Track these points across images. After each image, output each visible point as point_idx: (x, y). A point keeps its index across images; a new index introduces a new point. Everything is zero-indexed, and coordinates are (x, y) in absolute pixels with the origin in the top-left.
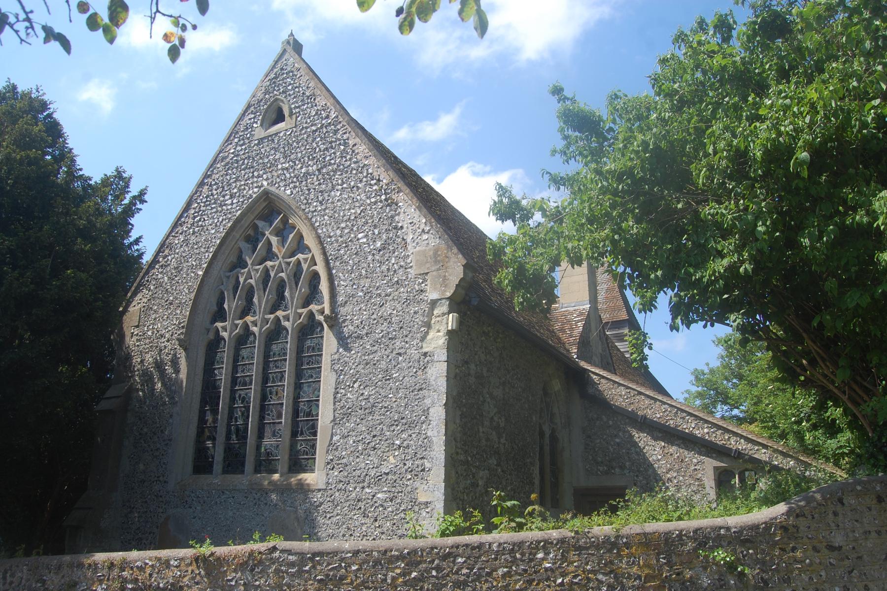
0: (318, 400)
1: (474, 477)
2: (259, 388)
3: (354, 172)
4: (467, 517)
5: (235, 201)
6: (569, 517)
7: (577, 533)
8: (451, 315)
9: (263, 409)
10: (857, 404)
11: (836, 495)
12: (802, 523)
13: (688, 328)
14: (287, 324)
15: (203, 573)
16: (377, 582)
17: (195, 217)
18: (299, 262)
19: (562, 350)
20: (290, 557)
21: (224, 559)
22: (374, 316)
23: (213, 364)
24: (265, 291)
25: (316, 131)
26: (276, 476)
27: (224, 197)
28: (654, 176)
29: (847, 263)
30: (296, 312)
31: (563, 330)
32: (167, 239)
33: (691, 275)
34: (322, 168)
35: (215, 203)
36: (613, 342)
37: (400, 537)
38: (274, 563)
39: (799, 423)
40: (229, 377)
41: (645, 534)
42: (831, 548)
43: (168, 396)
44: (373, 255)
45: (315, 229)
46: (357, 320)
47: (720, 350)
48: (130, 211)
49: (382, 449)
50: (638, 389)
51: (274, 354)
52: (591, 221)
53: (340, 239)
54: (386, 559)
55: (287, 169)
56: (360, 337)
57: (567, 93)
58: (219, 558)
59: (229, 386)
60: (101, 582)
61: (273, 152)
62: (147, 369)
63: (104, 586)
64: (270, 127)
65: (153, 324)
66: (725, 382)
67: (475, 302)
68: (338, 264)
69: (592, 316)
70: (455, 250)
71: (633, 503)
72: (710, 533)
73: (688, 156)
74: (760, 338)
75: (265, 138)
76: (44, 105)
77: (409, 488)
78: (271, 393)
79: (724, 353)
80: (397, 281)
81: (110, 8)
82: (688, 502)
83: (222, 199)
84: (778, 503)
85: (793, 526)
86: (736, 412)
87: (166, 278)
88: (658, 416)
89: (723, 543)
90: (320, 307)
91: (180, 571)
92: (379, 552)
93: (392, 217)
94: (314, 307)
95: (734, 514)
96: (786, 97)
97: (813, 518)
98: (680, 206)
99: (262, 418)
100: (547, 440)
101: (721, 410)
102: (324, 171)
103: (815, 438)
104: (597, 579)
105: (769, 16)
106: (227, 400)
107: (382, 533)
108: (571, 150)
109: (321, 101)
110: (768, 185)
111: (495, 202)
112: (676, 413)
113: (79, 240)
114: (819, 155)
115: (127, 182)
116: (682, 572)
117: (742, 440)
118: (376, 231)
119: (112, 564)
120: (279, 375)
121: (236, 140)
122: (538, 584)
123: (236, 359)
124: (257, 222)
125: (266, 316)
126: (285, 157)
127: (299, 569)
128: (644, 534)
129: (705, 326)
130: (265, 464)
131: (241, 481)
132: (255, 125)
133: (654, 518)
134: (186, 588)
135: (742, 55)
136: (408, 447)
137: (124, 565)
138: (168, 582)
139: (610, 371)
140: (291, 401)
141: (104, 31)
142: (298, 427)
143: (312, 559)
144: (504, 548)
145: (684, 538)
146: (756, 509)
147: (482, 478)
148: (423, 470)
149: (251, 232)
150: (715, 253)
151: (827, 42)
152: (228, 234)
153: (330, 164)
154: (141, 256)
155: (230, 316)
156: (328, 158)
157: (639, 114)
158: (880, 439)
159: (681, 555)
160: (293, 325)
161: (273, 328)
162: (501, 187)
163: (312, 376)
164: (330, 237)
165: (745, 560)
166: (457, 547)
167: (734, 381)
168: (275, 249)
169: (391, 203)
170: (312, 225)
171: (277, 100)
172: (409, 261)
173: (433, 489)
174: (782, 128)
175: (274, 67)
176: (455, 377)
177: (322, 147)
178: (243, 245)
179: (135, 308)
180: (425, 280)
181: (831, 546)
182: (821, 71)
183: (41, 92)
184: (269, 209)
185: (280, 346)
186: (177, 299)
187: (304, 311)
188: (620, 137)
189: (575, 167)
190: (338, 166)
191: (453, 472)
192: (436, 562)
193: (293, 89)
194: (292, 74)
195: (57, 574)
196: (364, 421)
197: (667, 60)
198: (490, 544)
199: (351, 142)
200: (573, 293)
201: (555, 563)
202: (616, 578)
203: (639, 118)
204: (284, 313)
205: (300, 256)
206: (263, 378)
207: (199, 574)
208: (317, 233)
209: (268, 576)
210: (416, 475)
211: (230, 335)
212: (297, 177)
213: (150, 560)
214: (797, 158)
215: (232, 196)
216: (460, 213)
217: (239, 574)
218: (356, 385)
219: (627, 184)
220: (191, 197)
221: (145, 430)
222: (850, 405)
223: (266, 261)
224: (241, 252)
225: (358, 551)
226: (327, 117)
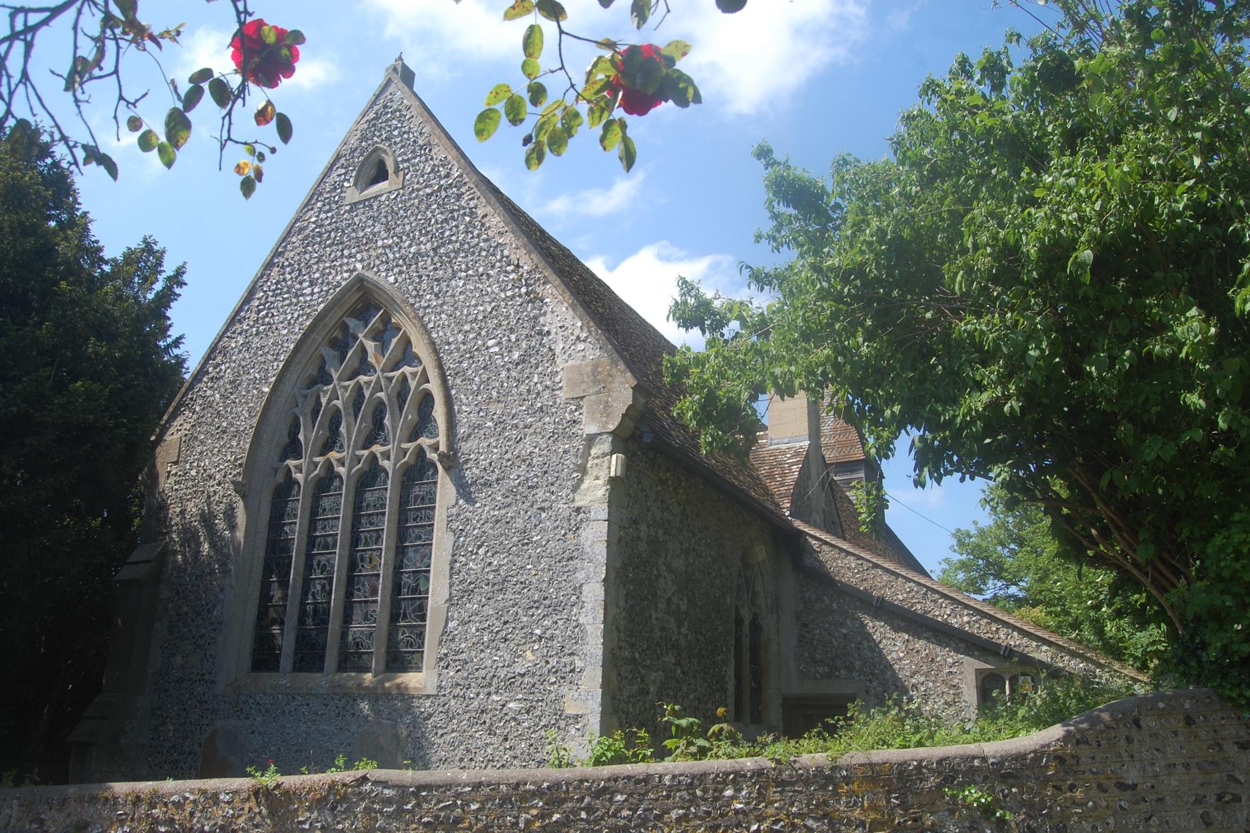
0: (428, 571)
1: (643, 680)
2: (346, 553)
3: (484, 253)
4: (630, 740)
6: (770, 738)
7: (778, 762)
8: (614, 456)
9: (351, 582)
10: (1163, 590)
11: (1131, 714)
12: (1085, 752)
13: (939, 481)
14: (386, 464)
15: (264, 811)
17: (259, 311)
18: (404, 378)
20: (386, 791)
21: (294, 793)
22: (508, 456)
23: (282, 517)
24: (356, 417)
25: (431, 194)
26: (369, 676)
27: (301, 283)
28: (893, 276)
29: (1146, 401)
30: (399, 447)
31: (771, 476)
33: (939, 415)
34: (439, 247)
35: (288, 292)
36: (844, 495)
38: (363, 799)
39: (1097, 607)
40: (305, 536)
41: (871, 765)
42: (1122, 786)
43: (218, 561)
44: (508, 370)
45: (428, 332)
48: (166, 297)
49: (516, 636)
50: (874, 560)
51: (368, 506)
52: (806, 337)
53: (463, 347)
54: (518, 795)
55: (390, 247)
56: (487, 484)
57: (778, 156)
58: (288, 792)
59: (304, 550)
60: (122, 823)
64: (367, 187)
65: (198, 460)
66: (999, 548)
67: (648, 439)
68: (458, 381)
69: (812, 459)
70: (622, 366)
71: (857, 721)
72: (959, 765)
73: (940, 249)
74: (1033, 499)
75: (359, 202)
78: (362, 560)
80: (541, 408)
81: (167, 124)
83: (298, 286)
84: (1054, 723)
85: (1073, 756)
86: (1013, 590)
87: (218, 396)
88: (901, 597)
89: (977, 779)
90: (432, 441)
92: (508, 785)
93: (536, 318)
94: (424, 441)
95: (995, 738)
96: (1069, 175)
97: (1099, 745)
98: (928, 315)
99: (349, 594)
100: (746, 630)
101: (993, 587)
102: (442, 250)
103: (1118, 630)
104: (805, 826)
105: (1054, 60)
106: (301, 569)
107: (515, 758)
109: (439, 153)
110: (1046, 292)
112: (926, 594)
113: (93, 340)
114: (1111, 256)
115: (160, 257)
116: (921, 818)
117: (1015, 633)
118: (513, 337)
119: (138, 797)
120: (375, 535)
121: (319, 204)
123: (314, 510)
125: (357, 453)
128: (871, 764)
129: (962, 480)
130: (351, 660)
131: (318, 681)
132: (346, 184)
133: (884, 743)
135: (1015, 113)
136: (552, 638)
137: (155, 800)
138: (215, 824)
139: (835, 534)
141: (160, 151)
142: (400, 608)
143: (416, 794)
146: (1023, 732)
147: (654, 682)
148: (572, 671)
149: (338, 334)
150: (971, 383)
152: (305, 336)
153: (450, 242)
155: (306, 451)
156: (448, 233)
157: (873, 190)
158: (1192, 639)
159: (920, 794)
160: (395, 465)
162: (685, 282)
163: (420, 538)
164: (449, 344)
166: (616, 780)
167: (1012, 546)
168: (371, 359)
169: (535, 299)
170: (424, 326)
171: (377, 149)
172: (557, 380)
173: (585, 697)
174: (1064, 217)
175: (374, 103)
177: (440, 217)
178: (328, 352)
179: (173, 436)
180: (579, 407)
182: (1117, 141)
184: (363, 301)
185: (377, 494)
186: (232, 425)
187: (411, 446)
188: (850, 218)
189: (789, 256)
190: (462, 245)
191: (614, 675)
193: (400, 135)
194: (398, 113)
195: (60, 811)
196: (491, 602)
197: (914, 118)
198: (660, 777)
199: (480, 212)
200: (785, 428)
203: (875, 195)
204: (383, 449)
205: (407, 369)
207: (260, 813)
208: (430, 337)
209: (356, 817)
210: (563, 678)
211: (306, 478)
212: (403, 258)
213: (192, 792)
215: (312, 283)
216: (631, 309)
217: (316, 814)
218: (481, 551)
219: (856, 287)
220: (255, 283)
221: (185, 609)
222: (1154, 592)
223: (358, 374)
224: (324, 361)
225: (480, 784)
226: (448, 176)
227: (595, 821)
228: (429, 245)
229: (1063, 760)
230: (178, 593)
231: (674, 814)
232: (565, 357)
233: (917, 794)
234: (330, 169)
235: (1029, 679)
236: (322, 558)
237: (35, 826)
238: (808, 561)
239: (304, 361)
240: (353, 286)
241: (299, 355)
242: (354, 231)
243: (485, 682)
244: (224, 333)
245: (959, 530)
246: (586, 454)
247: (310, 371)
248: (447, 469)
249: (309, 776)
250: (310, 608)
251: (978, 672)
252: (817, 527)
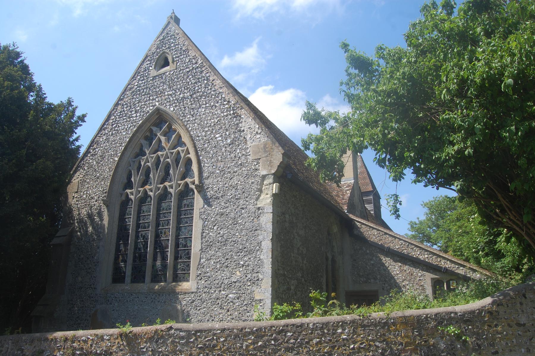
0: (191, 237)
1: (288, 284)
3: (213, 97)
5: (138, 115)
8: (275, 184)
15: (125, 343)
16: (237, 348)
17: (113, 125)
18: (178, 152)
19: (339, 207)
20: (181, 333)
21: (139, 335)
22: (227, 185)
23: (125, 215)
24: (157, 170)
25: (189, 71)
27: (131, 112)
30: (177, 183)
31: (338, 196)
32: (95, 138)
34: (193, 94)
35: (125, 116)
37: (244, 321)
38: (170, 337)
39: (477, 252)
41: (405, 317)
42: (519, 325)
43: (96, 235)
44: (226, 147)
45: (189, 132)
46: (216, 187)
47: (426, 210)
49: (231, 264)
50: (385, 231)
51: (163, 209)
53: (205, 138)
54: (242, 334)
55: (171, 95)
59: (135, 229)
60: (59, 350)
61: (162, 84)
62: (82, 219)
63: (61, 353)
64: (159, 70)
65: (87, 191)
66: (429, 229)
67: (289, 176)
68: (203, 153)
70: (277, 144)
75: (157, 76)
76: (18, 55)
77: (249, 291)
78: (161, 233)
79: (428, 212)
80: (241, 164)
82: (414, 298)
85: (496, 311)
87: (95, 162)
88: (397, 247)
90: (192, 180)
91: (110, 343)
93: (237, 124)
94: (188, 180)
97: (508, 306)
100: (330, 262)
104: (375, 345)
106: (134, 238)
107: (233, 319)
108: (352, 82)
109: (192, 53)
111: (305, 113)
112: (408, 245)
114: (520, 77)
116: (428, 340)
117: (448, 262)
118: (227, 133)
121: (139, 77)
122: (338, 349)
123: (139, 212)
124: (152, 127)
125: (158, 186)
126: (170, 88)
127: (187, 340)
128: (404, 317)
131: (142, 287)
133: (409, 307)
134: (114, 353)
136: (248, 265)
137: (74, 339)
138: (102, 350)
140: (174, 238)
142: (179, 254)
143: (195, 335)
144: (317, 326)
145: (429, 319)
147: (293, 285)
148: (258, 280)
149: (148, 134)
150: (447, 142)
151: (522, 8)
153: (198, 92)
154: (79, 147)
155: (135, 186)
156: (197, 88)
157: (397, 59)
160: (175, 191)
161: (162, 193)
162: (309, 103)
163: (187, 223)
164: (198, 137)
165: (466, 333)
166: (287, 326)
167: (434, 228)
168: (163, 144)
169: (237, 116)
170: (187, 129)
171: (164, 52)
172: (248, 151)
173: (264, 291)
175: (162, 32)
176: (277, 222)
177: (193, 81)
178: (144, 142)
179: (76, 179)
180: (258, 163)
181: (519, 324)
183: (16, 46)
184: (159, 119)
185: (167, 204)
186: (102, 175)
187: (182, 182)
190: (203, 93)
192: (274, 336)
193: (174, 46)
195: (31, 345)
196: (221, 250)
198: (308, 324)
199: (211, 79)
201: (349, 335)
202: (387, 344)
204: (169, 184)
205: (179, 149)
206: (156, 224)
207: (123, 344)
209: (167, 345)
212: (177, 100)
213: (91, 335)
214: (505, 83)
215: (136, 112)
217: (149, 344)
218: (215, 228)
219: (394, 99)
221: (82, 256)
225: (224, 329)
227: (278, 345)
228: (188, 94)
229: (491, 313)
230: (79, 249)
231: (315, 341)
232: (251, 141)
233: (426, 330)
234: (143, 62)
235: (455, 282)
236: (143, 233)
237: (19, 352)
238: (356, 232)
240: (155, 113)
242: (154, 88)
243: (218, 286)
244: (98, 133)
245: (411, 222)
246: (262, 184)
247: (136, 150)
248: (199, 192)
249: (145, 327)
251: (432, 279)
252: (357, 216)
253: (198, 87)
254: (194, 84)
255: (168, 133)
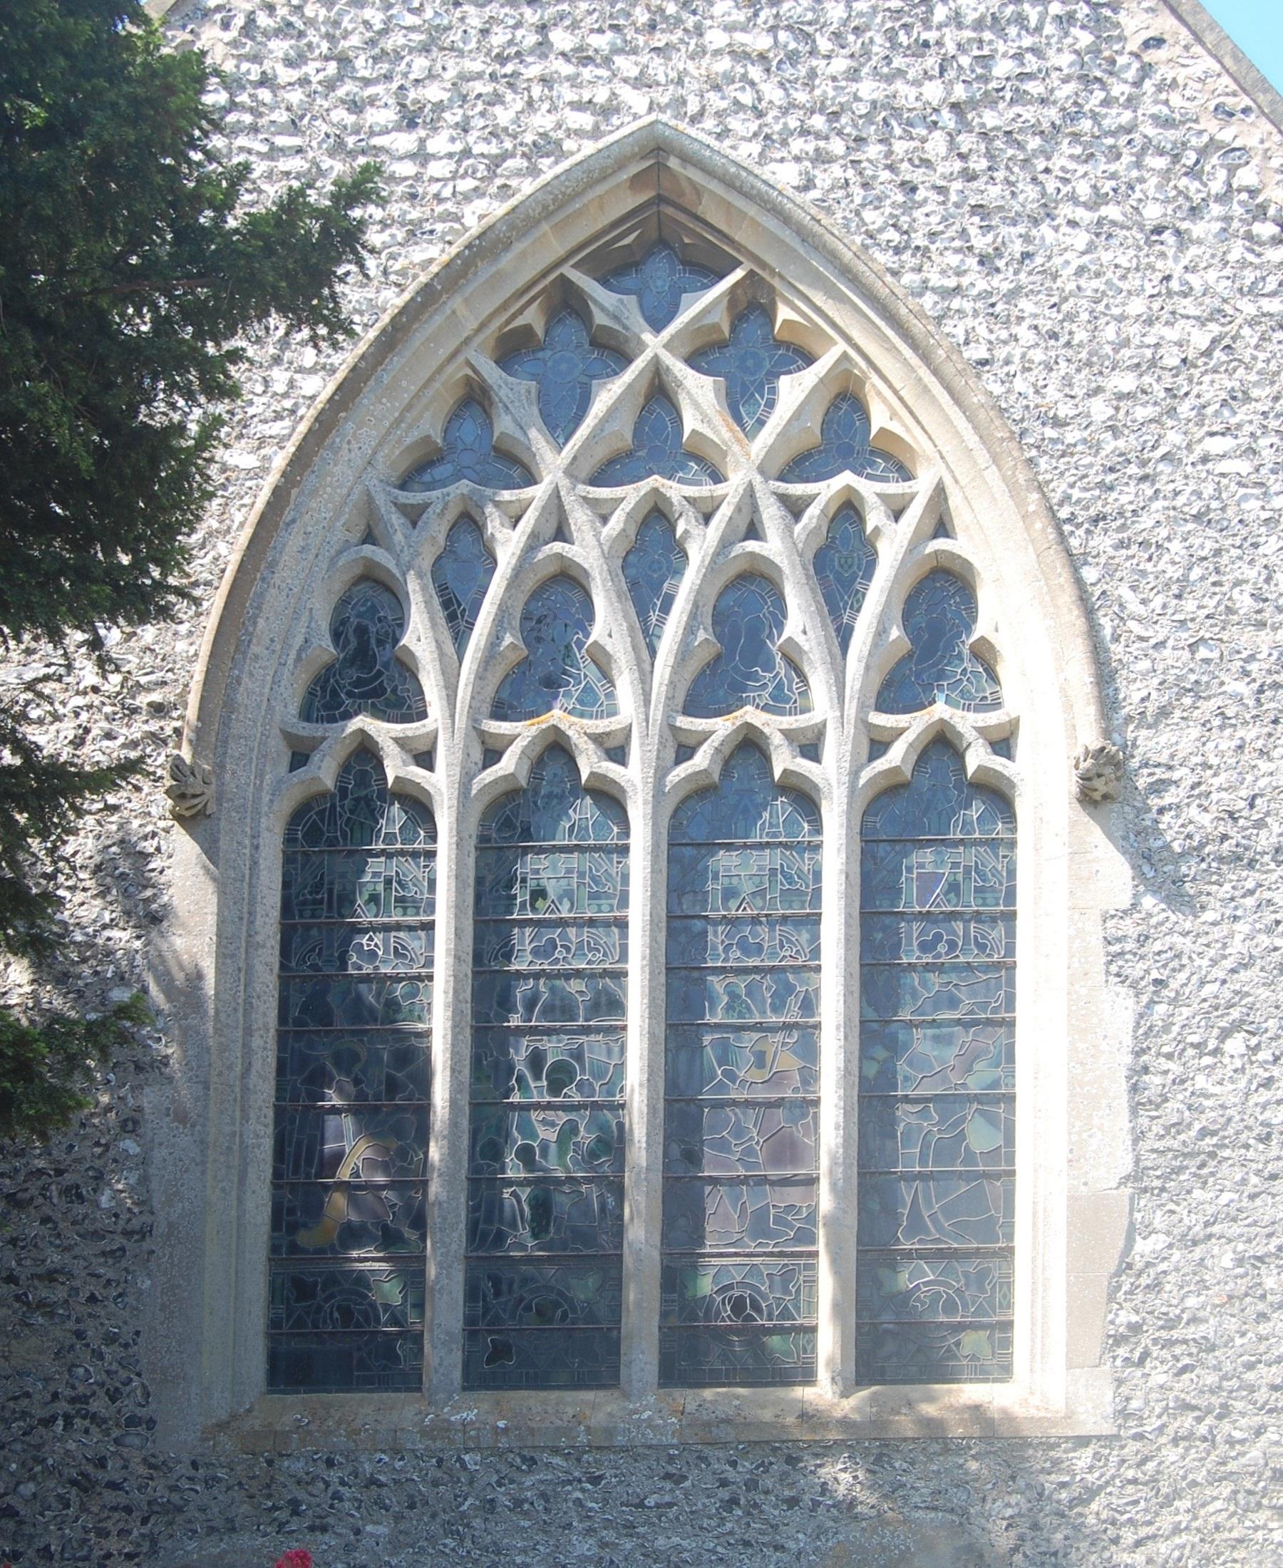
35: (294, 127)
53: (1110, 444)
153: (1019, 97)
239: (409, 388)
240: (621, 165)
241: (396, 362)
250: (516, 1199)
253: (1018, 57)
254: (979, 25)
255: (722, 345)
